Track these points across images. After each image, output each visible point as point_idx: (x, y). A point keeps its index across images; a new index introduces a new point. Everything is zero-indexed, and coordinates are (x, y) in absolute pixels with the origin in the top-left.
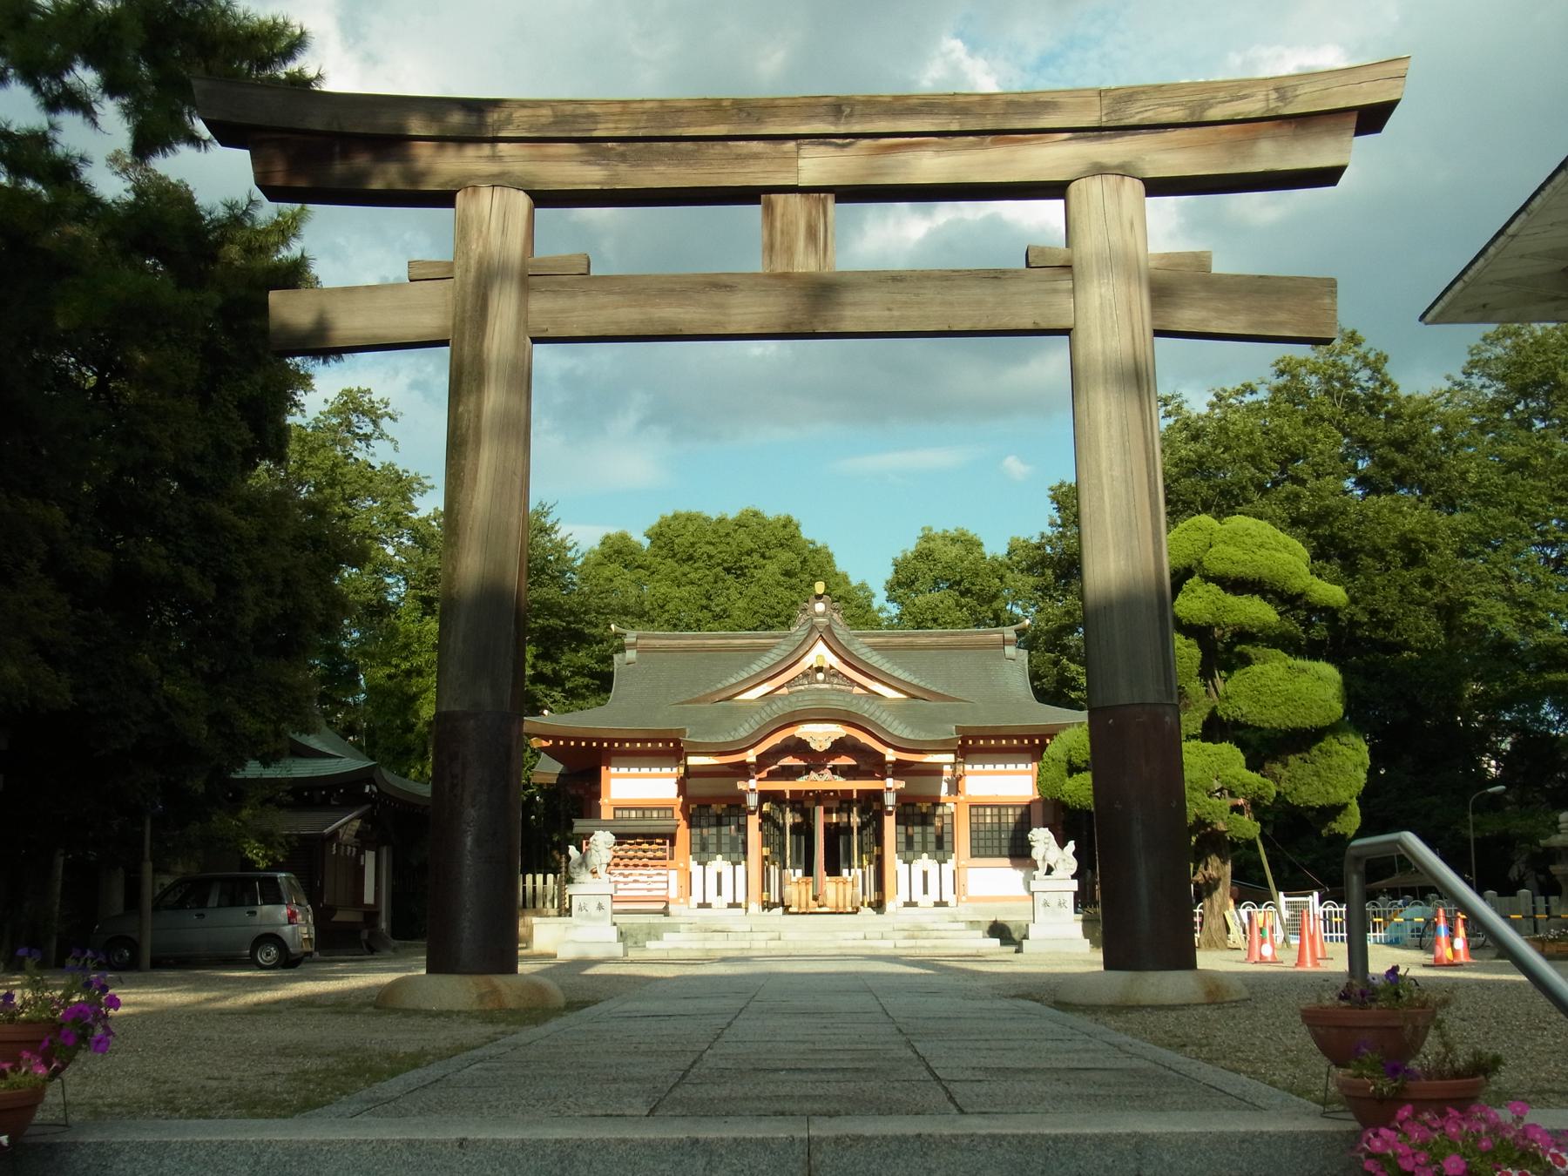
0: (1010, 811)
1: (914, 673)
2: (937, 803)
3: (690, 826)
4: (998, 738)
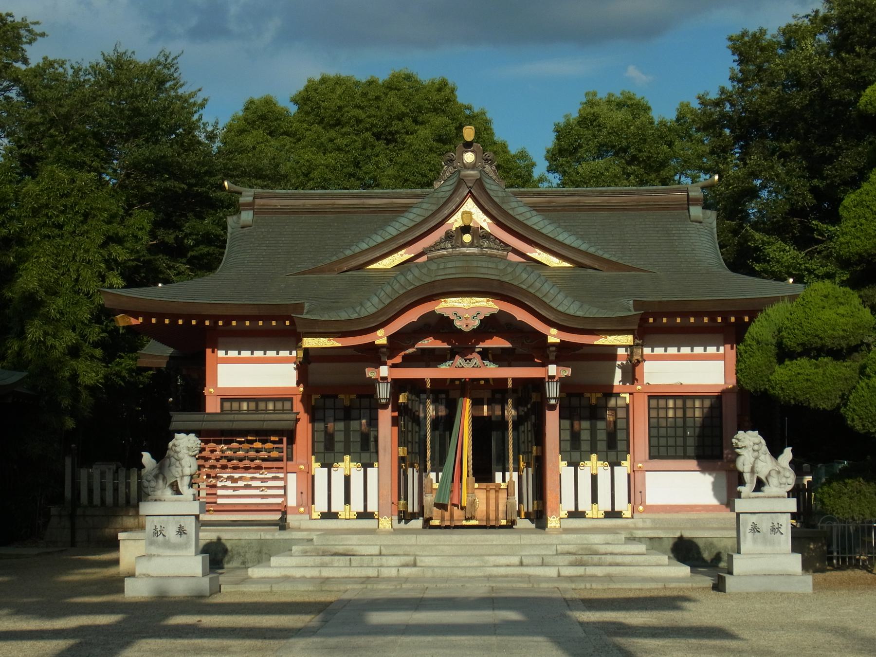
0: (698, 404)
1: (581, 237)
2: (609, 393)
3: (313, 420)
4: (267, 318)
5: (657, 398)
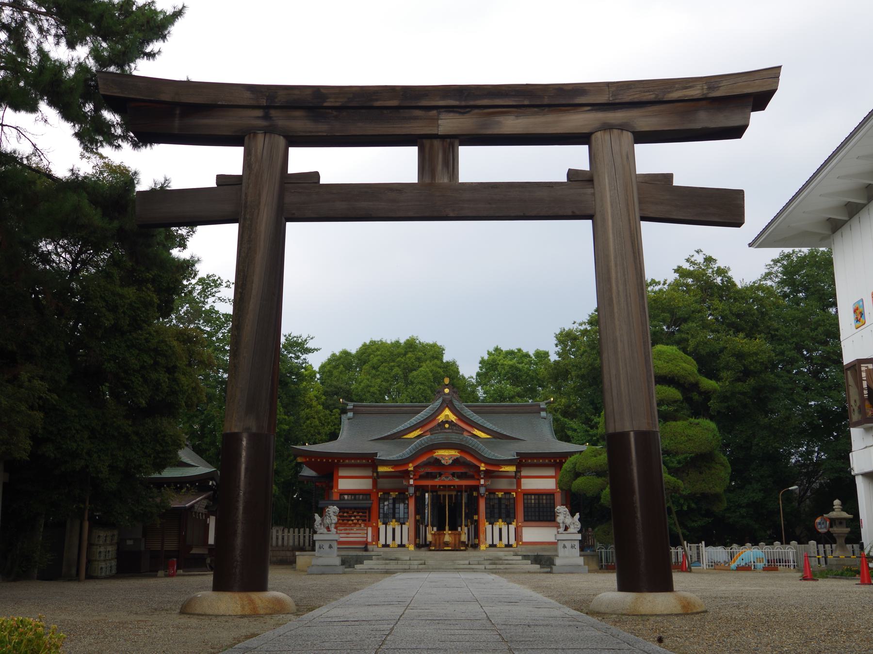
5: (528, 494)
